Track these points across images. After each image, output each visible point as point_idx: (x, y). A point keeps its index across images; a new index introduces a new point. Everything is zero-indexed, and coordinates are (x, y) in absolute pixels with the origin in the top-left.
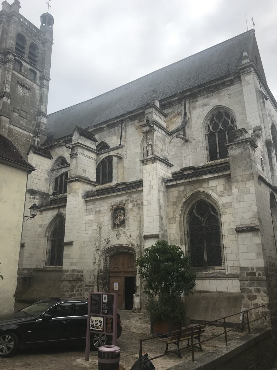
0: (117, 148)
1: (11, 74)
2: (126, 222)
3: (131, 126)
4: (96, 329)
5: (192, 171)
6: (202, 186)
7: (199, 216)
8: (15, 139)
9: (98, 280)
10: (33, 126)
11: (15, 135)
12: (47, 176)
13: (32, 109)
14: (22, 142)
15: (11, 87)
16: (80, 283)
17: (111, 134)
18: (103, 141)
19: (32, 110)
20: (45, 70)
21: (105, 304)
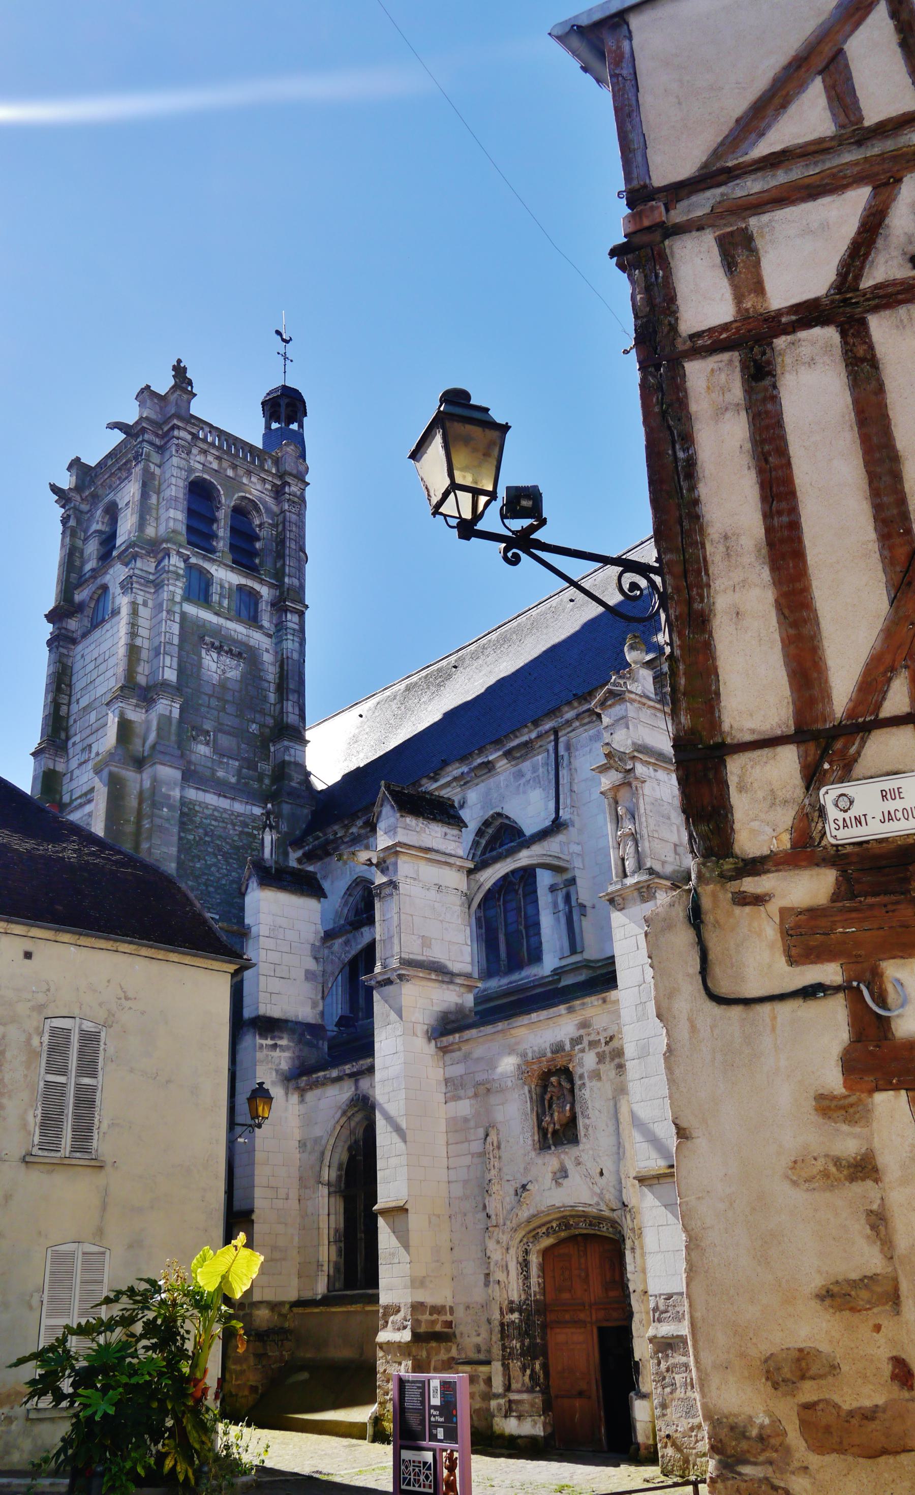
0: (543, 835)
1: (177, 618)
2: (581, 1122)
3: (588, 749)
4: (417, 1489)
8: (206, 834)
9: (502, 1339)
10: (260, 780)
11: (204, 821)
12: (311, 965)
13: (254, 722)
14: (230, 841)
15: (179, 665)
16: (443, 1351)
18: (498, 810)
19: (254, 726)
20: (286, 580)
21: (435, 1410)
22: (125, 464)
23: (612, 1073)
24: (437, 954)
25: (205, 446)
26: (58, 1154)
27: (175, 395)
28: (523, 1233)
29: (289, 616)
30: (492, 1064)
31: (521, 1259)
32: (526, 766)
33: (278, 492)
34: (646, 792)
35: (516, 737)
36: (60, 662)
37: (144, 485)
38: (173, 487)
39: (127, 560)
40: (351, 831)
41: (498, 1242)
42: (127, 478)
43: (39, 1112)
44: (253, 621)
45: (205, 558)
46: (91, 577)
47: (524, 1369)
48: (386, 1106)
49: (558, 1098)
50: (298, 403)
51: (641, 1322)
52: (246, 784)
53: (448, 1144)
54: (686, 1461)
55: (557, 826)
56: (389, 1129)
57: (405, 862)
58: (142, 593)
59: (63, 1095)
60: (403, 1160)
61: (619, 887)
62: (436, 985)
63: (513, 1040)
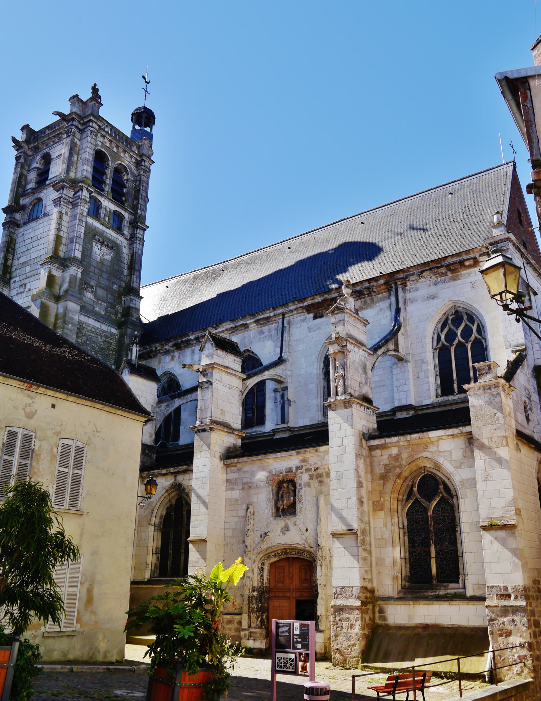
1: (84, 225)
2: (298, 506)
3: (299, 325)
4: (285, 669)
5: (411, 413)
6: (428, 449)
7: (423, 500)
8: (87, 340)
9: (249, 604)
10: (116, 314)
13: (115, 284)
15: (83, 248)
17: (263, 336)
18: (249, 348)
19: (115, 286)
20: (139, 211)
22: (58, 134)
23: (317, 484)
24: (227, 419)
25: (104, 134)
26: (63, 507)
27: (92, 103)
28: (262, 555)
29: (138, 231)
30: (253, 475)
31: (260, 567)
32: (265, 328)
33: (138, 164)
34: (351, 357)
35: (263, 314)
36: (9, 236)
37: (71, 149)
38: (87, 153)
39: (58, 188)
40: (165, 347)
41: (250, 559)
42: (57, 142)
43: (55, 486)
44: (119, 229)
45: (99, 193)
46: (32, 193)
47: (257, 618)
48: (198, 491)
49: (286, 494)
50: (151, 118)
51: (322, 598)
52: (109, 316)
53: (225, 511)
54: (345, 660)
55: (280, 361)
56: (199, 502)
57: (216, 372)
58: (65, 208)
59: (66, 478)
60: (206, 517)
61: (334, 400)
62: (226, 434)
63: (265, 464)
